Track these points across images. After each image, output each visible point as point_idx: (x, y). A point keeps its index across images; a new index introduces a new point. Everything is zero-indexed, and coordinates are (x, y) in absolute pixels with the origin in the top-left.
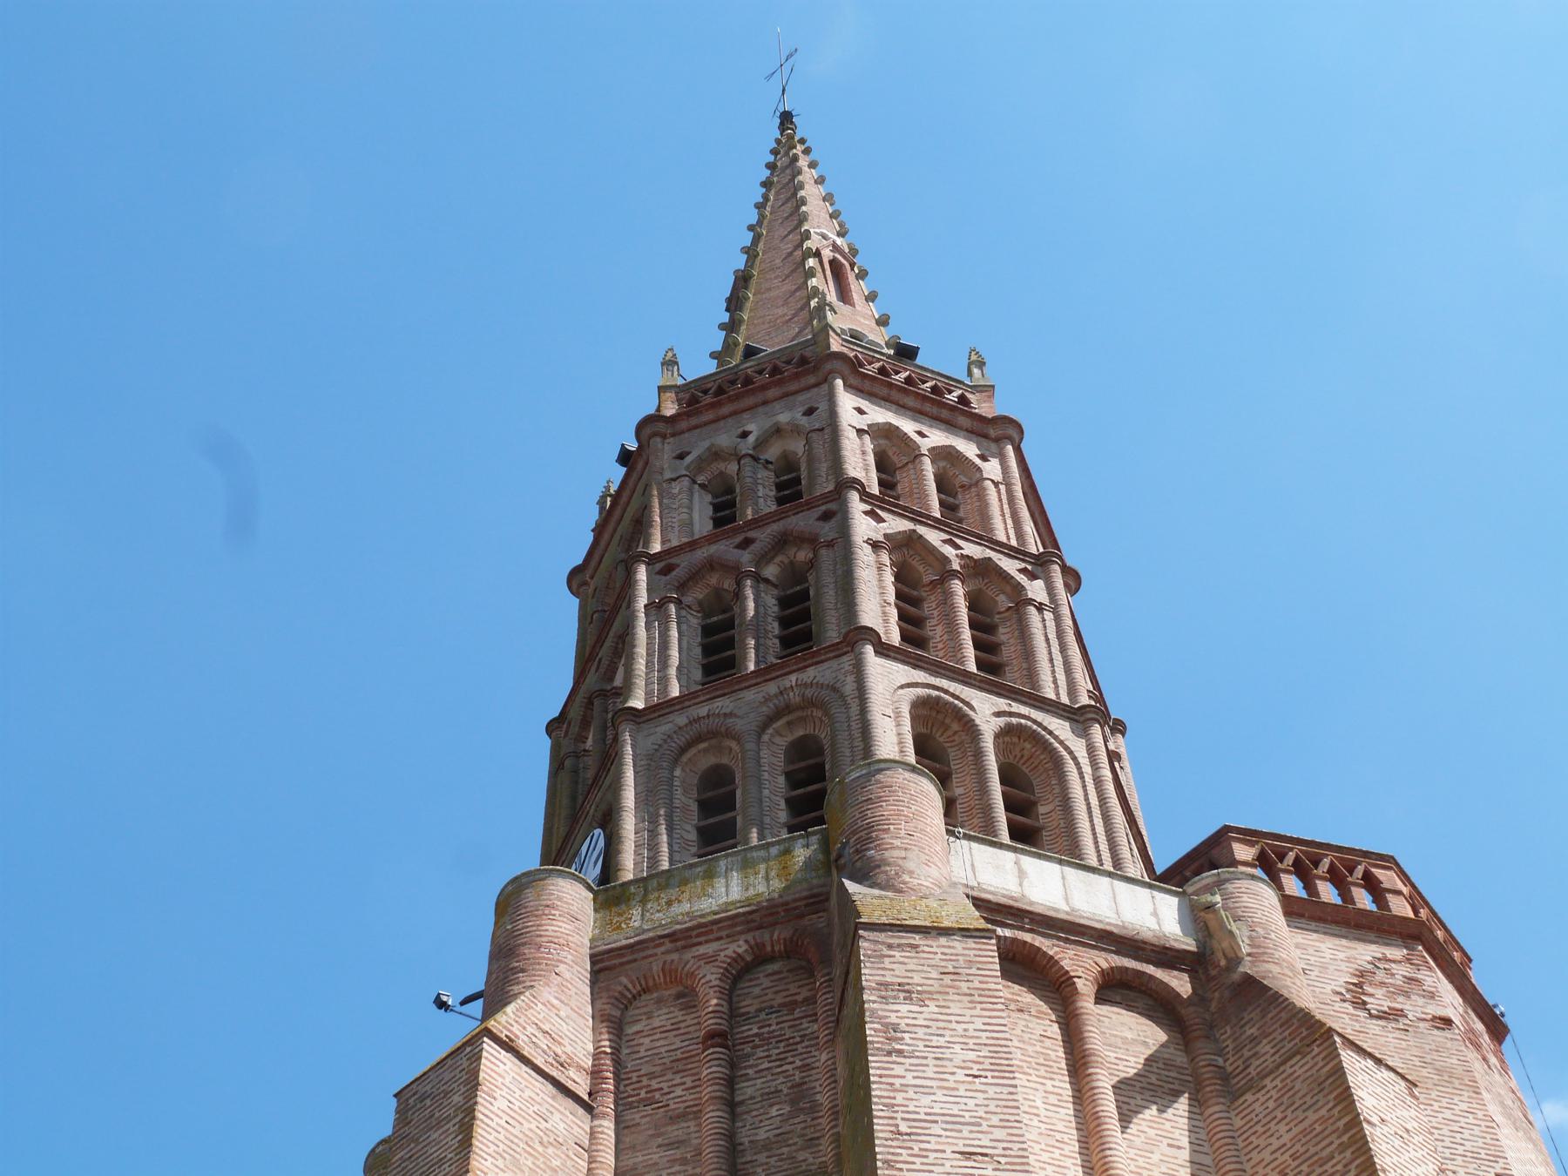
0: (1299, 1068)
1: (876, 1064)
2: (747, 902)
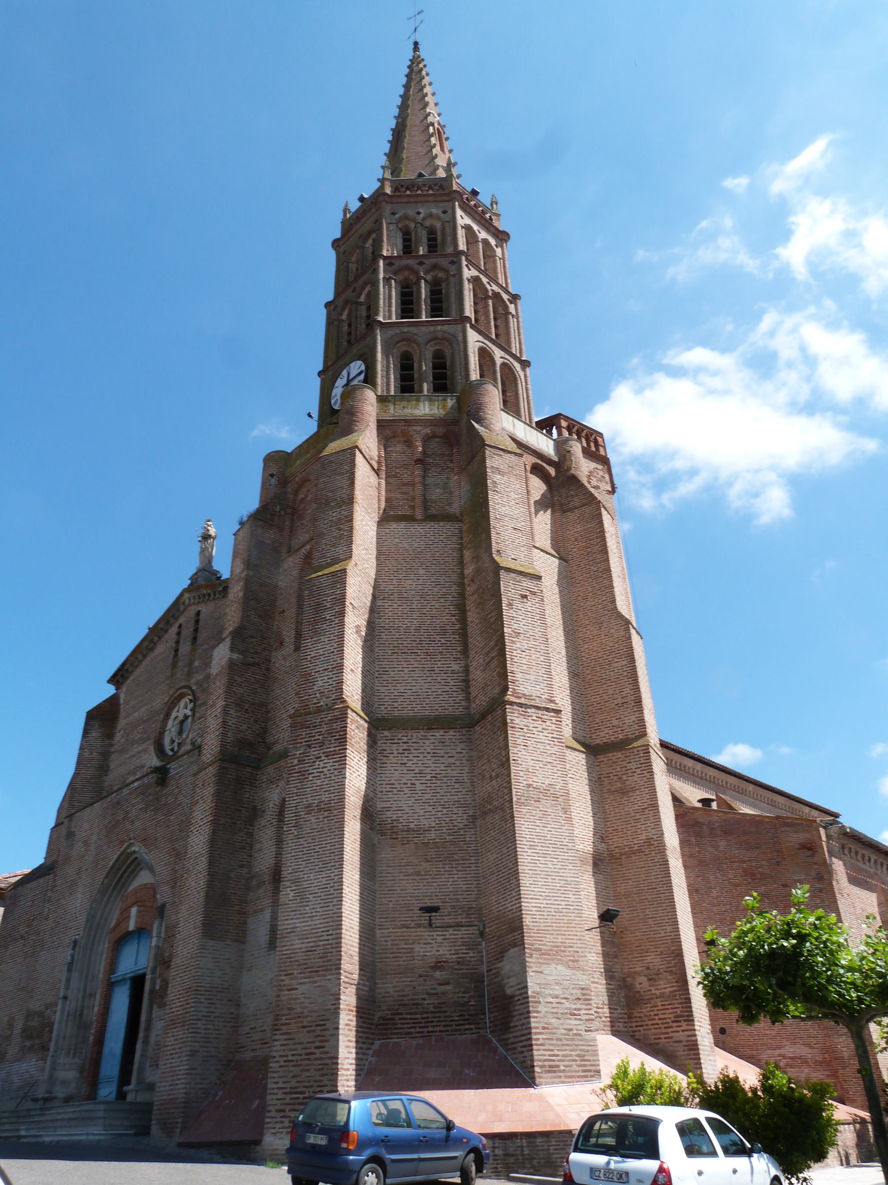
0: (587, 510)
1: (491, 494)
2: (431, 415)
